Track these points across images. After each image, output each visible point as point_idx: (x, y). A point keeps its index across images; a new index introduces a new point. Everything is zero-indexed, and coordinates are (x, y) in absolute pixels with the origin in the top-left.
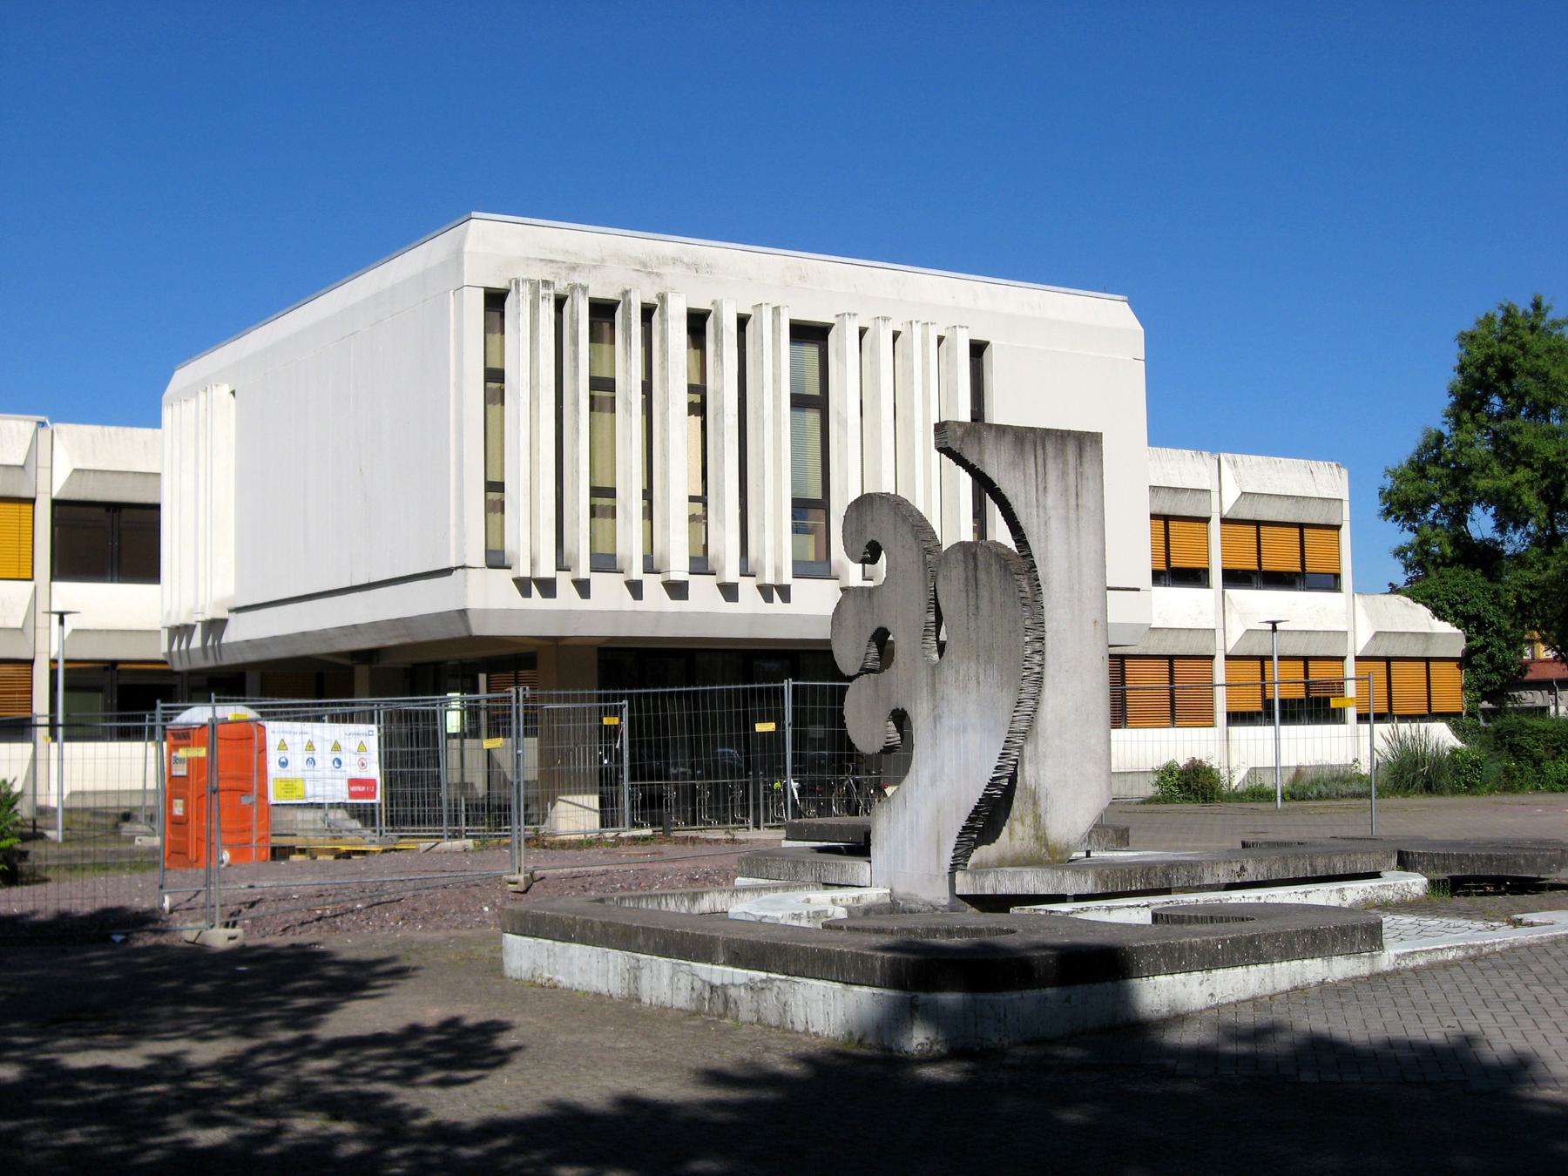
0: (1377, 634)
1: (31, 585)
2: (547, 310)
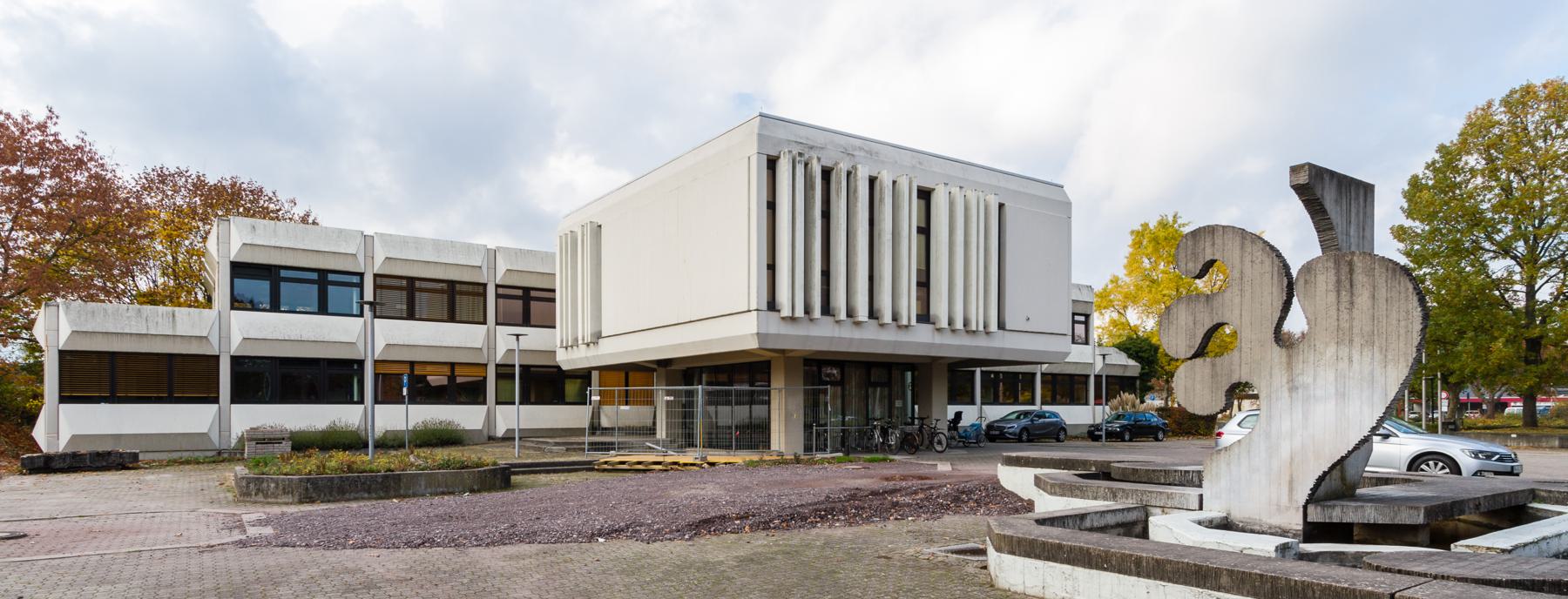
0: (74, 437)
1: (215, 406)
2: (800, 169)
